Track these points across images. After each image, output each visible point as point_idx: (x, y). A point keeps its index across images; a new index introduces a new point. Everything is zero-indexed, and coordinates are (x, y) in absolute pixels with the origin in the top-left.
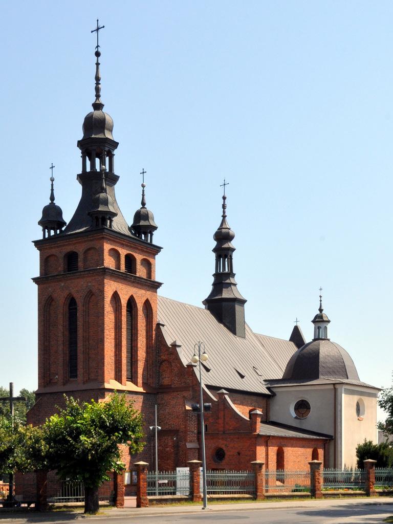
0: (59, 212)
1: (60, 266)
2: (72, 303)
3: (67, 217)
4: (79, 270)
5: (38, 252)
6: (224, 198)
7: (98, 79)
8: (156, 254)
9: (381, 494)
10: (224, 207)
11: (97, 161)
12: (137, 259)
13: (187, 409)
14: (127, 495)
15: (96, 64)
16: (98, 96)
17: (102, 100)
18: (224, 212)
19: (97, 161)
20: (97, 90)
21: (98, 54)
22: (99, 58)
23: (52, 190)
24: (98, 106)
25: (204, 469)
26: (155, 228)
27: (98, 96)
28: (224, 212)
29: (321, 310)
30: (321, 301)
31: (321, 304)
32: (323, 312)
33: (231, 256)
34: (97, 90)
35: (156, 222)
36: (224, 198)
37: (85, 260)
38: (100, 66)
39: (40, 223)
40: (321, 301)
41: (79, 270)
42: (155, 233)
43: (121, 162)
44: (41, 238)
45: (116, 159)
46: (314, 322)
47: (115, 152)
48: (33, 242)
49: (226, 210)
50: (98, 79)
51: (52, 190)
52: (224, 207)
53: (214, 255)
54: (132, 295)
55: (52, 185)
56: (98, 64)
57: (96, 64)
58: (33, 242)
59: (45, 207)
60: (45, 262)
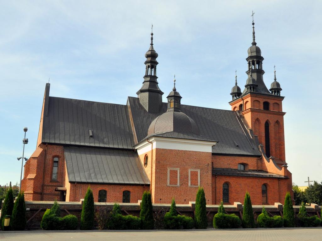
0: (239, 89)
4: (243, 104)
5: (286, 162)
6: (152, 34)
7: (254, 33)
10: (152, 39)
11: (253, 68)
13: (16, 197)
16: (254, 40)
18: (152, 42)
19: (253, 68)
20: (254, 37)
21: (253, 24)
24: (254, 44)
27: (254, 40)
28: (152, 42)
33: (156, 67)
34: (254, 37)
36: (152, 34)
39: (281, 89)
41: (243, 104)
49: (153, 41)
50: (254, 33)
52: (152, 39)
56: (254, 28)
57: (153, 44)
59: (291, 174)
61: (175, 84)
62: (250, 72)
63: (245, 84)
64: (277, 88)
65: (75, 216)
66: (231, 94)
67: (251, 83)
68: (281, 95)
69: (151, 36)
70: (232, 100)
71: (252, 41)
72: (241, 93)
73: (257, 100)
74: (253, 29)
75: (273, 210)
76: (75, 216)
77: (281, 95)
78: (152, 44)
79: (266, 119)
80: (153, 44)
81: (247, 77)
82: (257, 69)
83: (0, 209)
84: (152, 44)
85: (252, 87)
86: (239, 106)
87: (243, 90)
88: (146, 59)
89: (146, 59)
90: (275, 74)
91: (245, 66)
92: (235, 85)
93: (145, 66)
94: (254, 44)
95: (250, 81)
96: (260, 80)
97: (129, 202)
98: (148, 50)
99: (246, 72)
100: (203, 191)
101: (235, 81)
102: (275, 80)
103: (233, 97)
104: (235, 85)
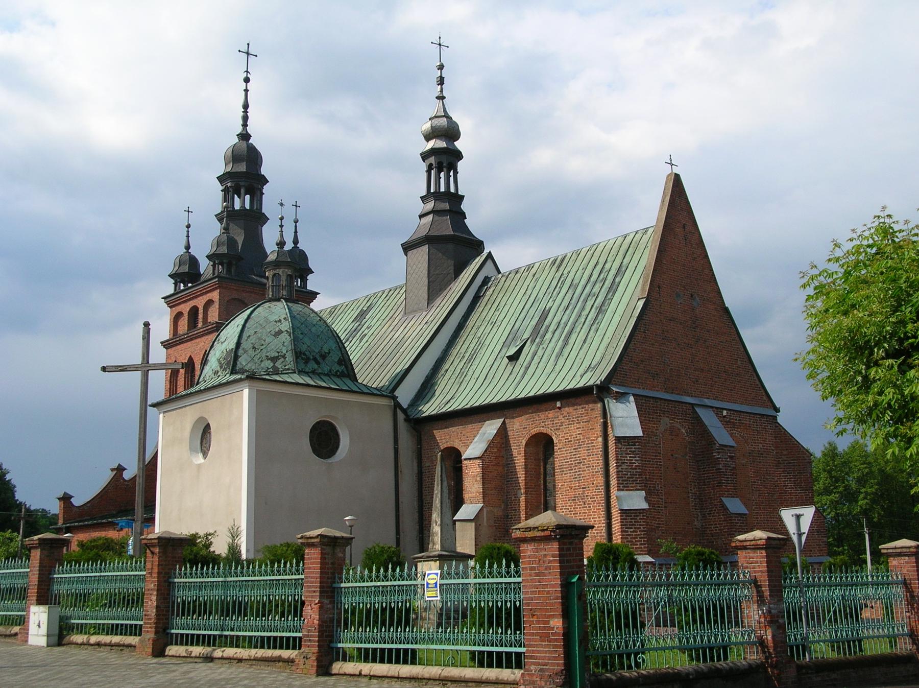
7: (246, 106)
12: (188, 310)
16: (245, 125)
20: (245, 118)
23: (296, 232)
24: (245, 136)
27: (245, 125)
34: (245, 118)
50: (246, 106)
51: (296, 232)
55: (296, 226)
56: (246, 91)
57: (248, 91)
61: (281, 226)
62: (228, 216)
63: (208, 250)
66: (171, 276)
67: (224, 250)
68: (310, 287)
70: (172, 291)
71: (239, 129)
72: (200, 275)
73: (233, 299)
74: (244, 93)
77: (310, 287)
80: (244, 90)
81: (216, 229)
83: (917, 513)
87: (205, 265)
90: (188, 231)
92: (185, 251)
93: (424, 166)
94: (245, 136)
95: (223, 244)
96: (254, 239)
99: (216, 216)
100: (326, 540)
101: (185, 238)
102: (188, 247)
103: (175, 284)
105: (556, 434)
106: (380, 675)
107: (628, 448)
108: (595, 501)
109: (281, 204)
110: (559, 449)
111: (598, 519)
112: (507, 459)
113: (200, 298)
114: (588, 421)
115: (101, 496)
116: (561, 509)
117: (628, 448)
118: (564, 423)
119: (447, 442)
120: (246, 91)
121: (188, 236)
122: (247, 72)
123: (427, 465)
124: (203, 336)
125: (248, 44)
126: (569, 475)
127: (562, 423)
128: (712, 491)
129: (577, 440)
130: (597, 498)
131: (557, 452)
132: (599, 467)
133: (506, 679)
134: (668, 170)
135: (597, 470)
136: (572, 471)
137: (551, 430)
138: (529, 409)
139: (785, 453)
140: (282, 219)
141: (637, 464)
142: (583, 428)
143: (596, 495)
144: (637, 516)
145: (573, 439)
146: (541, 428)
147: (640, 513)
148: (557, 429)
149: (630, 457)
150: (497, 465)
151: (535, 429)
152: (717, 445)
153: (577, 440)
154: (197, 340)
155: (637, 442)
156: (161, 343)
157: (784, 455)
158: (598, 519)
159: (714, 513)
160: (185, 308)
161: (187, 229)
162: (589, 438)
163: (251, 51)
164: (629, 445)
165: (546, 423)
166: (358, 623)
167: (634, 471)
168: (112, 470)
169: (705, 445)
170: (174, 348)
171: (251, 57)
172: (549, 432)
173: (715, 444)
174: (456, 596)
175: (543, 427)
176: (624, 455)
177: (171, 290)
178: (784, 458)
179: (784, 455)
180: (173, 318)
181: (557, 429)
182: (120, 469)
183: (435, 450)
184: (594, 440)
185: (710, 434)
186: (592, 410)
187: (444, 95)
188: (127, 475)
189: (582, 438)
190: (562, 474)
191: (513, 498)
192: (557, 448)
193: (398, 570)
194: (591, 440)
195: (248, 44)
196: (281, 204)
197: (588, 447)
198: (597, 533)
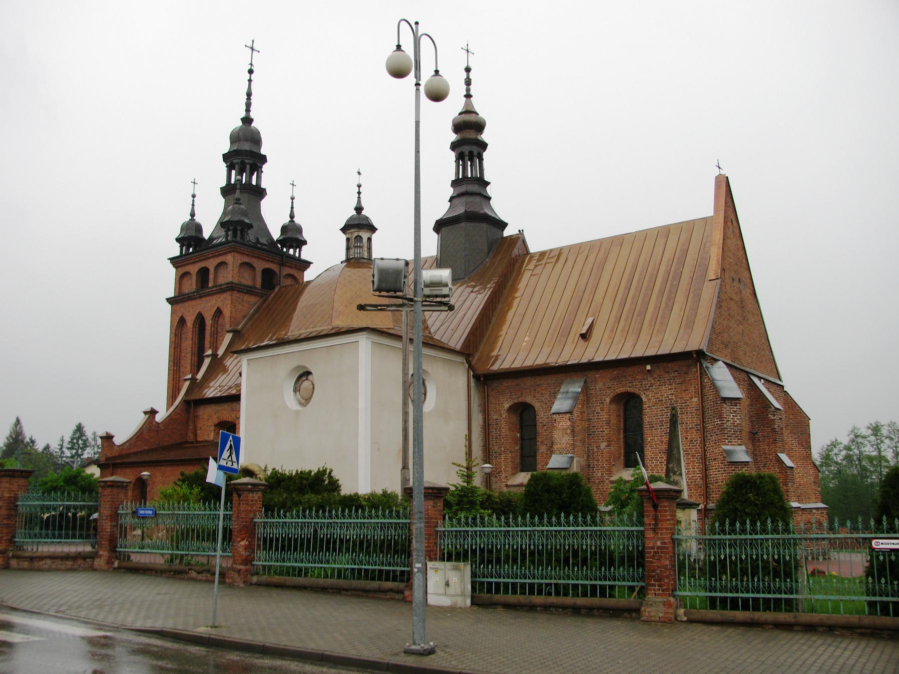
0: (199, 228)
1: (191, 285)
2: (200, 319)
3: (206, 235)
6: (468, 70)
7: (249, 95)
8: (305, 270)
9: (219, 521)
12: (197, 270)
14: (434, 554)
15: (249, 80)
16: (248, 110)
17: (252, 115)
18: (468, 90)
20: (248, 105)
21: (251, 72)
22: (252, 75)
23: (292, 208)
24: (247, 120)
25: (727, 578)
26: (305, 243)
27: (248, 110)
28: (468, 90)
29: (359, 209)
30: (359, 193)
31: (359, 198)
32: (363, 213)
34: (248, 105)
35: (306, 235)
36: (468, 70)
37: (215, 277)
38: (252, 83)
40: (359, 193)
42: (304, 248)
43: (269, 177)
44: (178, 254)
45: (264, 176)
46: (344, 230)
47: (486, 155)
48: (169, 259)
50: (249, 95)
51: (292, 208)
52: (468, 82)
53: (452, 155)
54: (200, 312)
56: (250, 81)
57: (249, 80)
58: (169, 259)
59: (437, 222)
60: (181, 279)
64: (194, 234)
65: (400, 497)
68: (303, 257)
69: (465, 75)
71: (243, 114)
74: (248, 83)
75: (453, 668)
76: (400, 497)
78: (468, 96)
79: (197, 312)
81: (220, 203)
82: (468, 178)
84: (468, 96)
85: (238, 228)
86: (198, 272)
88: (453, 137)
89: (453, 137)
91: (219, 175)
94: (247, 120)
97: (218, 443)
98: (460, 110)
102: (193, 215)
104: (190, 218)
105: (645, 394)
106: (730, 631)
107: (732, 408)
108: (689, 454)
109: (359, 173)
110: (648, 407)
111: (692, 470)
112: (588, 414)
113: (211, 260)
114: (682, 384)
115: (138, 437)
116: (650, 461)
117: (732, 408)
118: (653, 384)
119: (518, 398)
120: (250, 81)
121: (193, 205)
122: (251, 64)
123: (495, 417)
124: (215, 294)
125: (253, 41)
126: (600, 430)
127: (651, 384)
128: (767, 447)
129: (669, 399)
130: (691, 451)
131: (646, 409)
132: (694, 424)
133: (481, 609)
134: (717, 172)
135: (691, 426)
136: (663, 427)
137: (639, 390)
138: (614, 371)
139: (791, 417)
140: (359, 186)
141: (738, 422)
142: (675, 389)
143: (689, 449)
144: (743, 468)
145: (664, 399)
146: (629, 388)
147: (745, 465)
148: (646, 390)
149: (733, 416)
150: (581, 420)
151: (621, 389)
152: (773, 408)
153: (669, 399)
154: (208, 298)
155: (738, 403)
156: (167, 299)
157: (791, 419)
158: (692, 470)
159: (769, 466)
160: (194, 269)
161: (192, 199)
162: (683, 398)
163: (255, 47)
164: (732, 405)
165: (634, 384)
166: (730, 575)
167: (737, 428)
168: (145, 413)
169: (760, 408)
170: (180, 305)
171: (255, 53)
172: (637, 391)
173: (770, 407)
174: (575, 541)
175: (630, 387)
176: (728, 414)
177: (177, 253)
178: (791, 421)
179: (791, 419)
180: (178, 277)
181: (646, 390)
182: (153, 413)
183: (504, 405)
184: (688, 400)
185: (765, 398)
186: (685, 373)
187: (465, 99)
188: (159, 418)
189: (674, 397)
190: (651, 430)
191: (596, 450)
192: (646, 406)
193: (360, 511)
194: (685, 400)
195: (253, 41)
196: (359, 173)
197: (682, 406)
198: (691, 482)
